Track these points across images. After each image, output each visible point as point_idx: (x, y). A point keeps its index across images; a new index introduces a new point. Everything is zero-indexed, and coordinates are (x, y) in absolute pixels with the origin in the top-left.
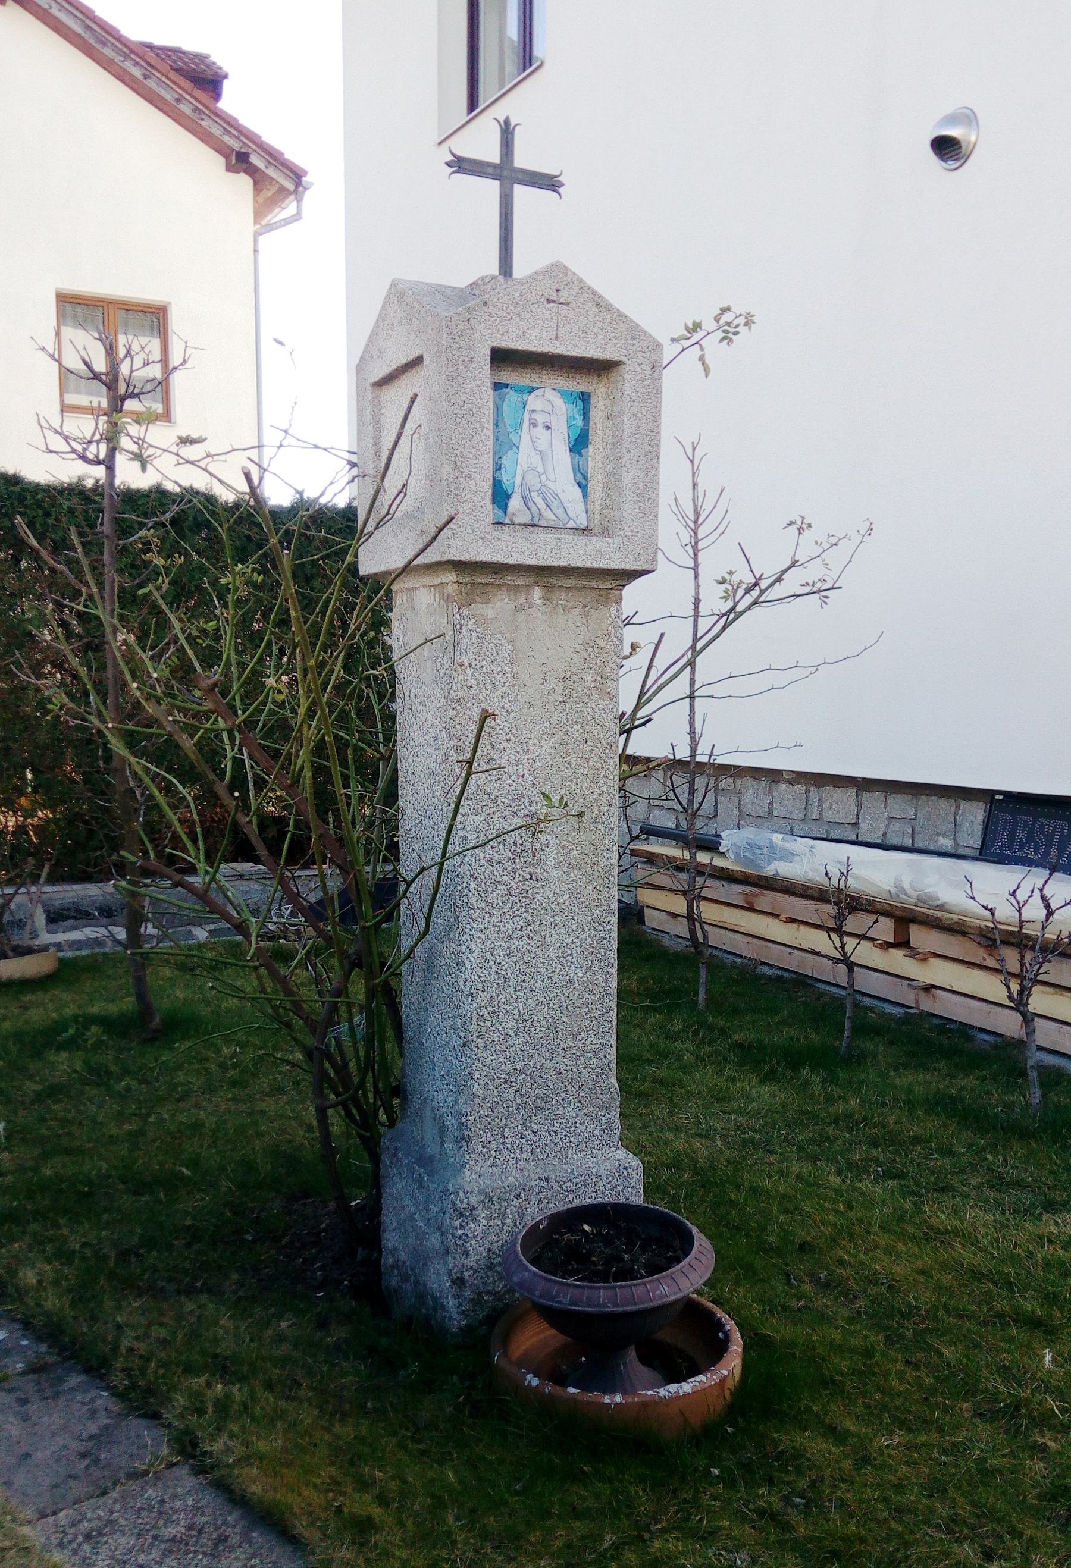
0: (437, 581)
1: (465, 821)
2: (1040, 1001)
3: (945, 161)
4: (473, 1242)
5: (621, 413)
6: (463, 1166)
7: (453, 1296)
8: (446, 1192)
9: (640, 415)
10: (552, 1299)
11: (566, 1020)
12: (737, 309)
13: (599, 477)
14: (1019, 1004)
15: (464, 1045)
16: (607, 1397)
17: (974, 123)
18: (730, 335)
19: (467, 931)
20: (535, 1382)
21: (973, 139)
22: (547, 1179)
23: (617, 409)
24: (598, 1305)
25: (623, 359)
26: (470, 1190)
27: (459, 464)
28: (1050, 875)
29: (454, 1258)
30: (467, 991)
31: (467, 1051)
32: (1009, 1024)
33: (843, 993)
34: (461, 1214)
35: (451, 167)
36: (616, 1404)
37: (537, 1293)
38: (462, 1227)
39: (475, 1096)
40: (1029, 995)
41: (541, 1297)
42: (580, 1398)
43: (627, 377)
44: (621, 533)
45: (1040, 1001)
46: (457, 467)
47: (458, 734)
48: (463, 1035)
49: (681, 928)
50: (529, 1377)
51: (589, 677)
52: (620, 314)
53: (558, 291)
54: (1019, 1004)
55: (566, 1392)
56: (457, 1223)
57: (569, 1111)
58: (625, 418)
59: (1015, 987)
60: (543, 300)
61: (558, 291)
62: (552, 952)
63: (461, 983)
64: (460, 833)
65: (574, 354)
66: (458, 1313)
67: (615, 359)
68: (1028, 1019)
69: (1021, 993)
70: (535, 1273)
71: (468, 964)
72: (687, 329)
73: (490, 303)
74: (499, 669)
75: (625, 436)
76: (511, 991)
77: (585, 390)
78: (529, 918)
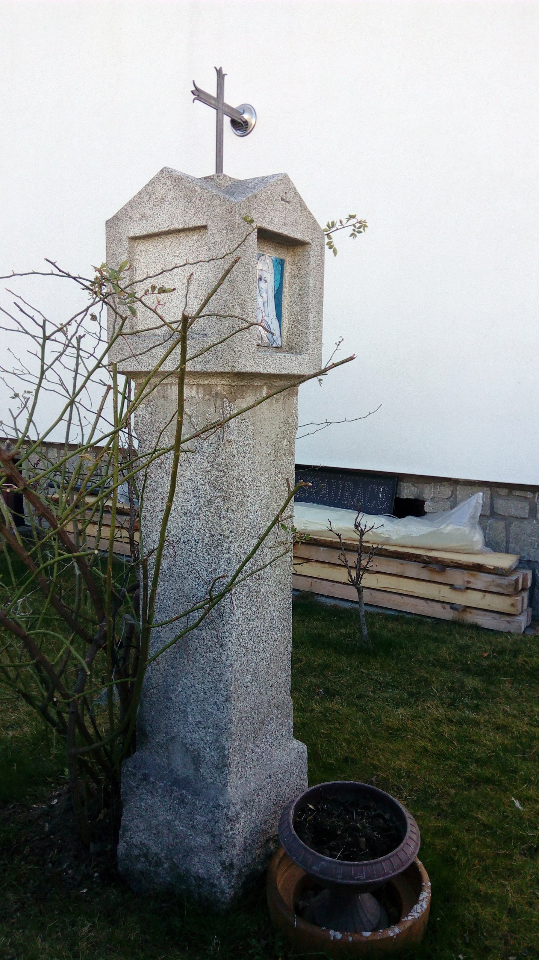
0: (207, 382)
1: (229, 547)
2: (367, 580)
3: (236, 130)
4: (238, 837)
5: (307, 275)
6: (225, 785)
7: (225, 877)
8: (218, 806)
9: (316, 278)
10: (352, 878)
11: (272, 666)
12: (359, 218)
13: (287, 314)
14: (356, 583)
15: (226, 701)
16: (390, 932)
17: (254, 115)
18: (356, 233)
19: (230, 622)
20: (339, 936)
21: (253, 123)
22: (270, 776)
23: (303, 272)
24: (385, 874)
25: (311, 241)
26: (235, 801)
27: (243, 305)
28: (359, 514)
29: (227, 852)
30: (228, 663)
31: (228, 704)
32: (352, 593)
33: (357, 606)
34: (231, 820)
35: (194, 94)
36: (397, 935)
37: (340, 876)
38: (232, 829)
39: (232, 734)
40: (361, 578)
41: (344, 878)
42: (375, 938)
43: (312, 253)
44: (308, 352)
45: (367, 580)
46: (242, 308)
47: (225, 488)
48: (225, 694)
49: (126, 549)
50: (332, 932)
51: (285, 443)
52: (310, 213)
53: (286, 193)
54: (356, 583)
55: (362, 936)
56: (228, 828)
57: (273, 725)
58: (311, 279)
59: (354, 574)
60: (280, 198)
61: (286, 193)
62: (267, 624)
63: (224, 658)
64: (226, 556)
65: (292, 236)
66: (229, 888)
67: (308, 241)
68: (359, 591)
69: (358, 578)
70: (331, 862)
71: (230, 645)
72: (328, 226)
73: (258, 196)
74: (247, 442)
75: (310, 291)
76: (249, 656)
77: (282, 258)
78: (258, 605)
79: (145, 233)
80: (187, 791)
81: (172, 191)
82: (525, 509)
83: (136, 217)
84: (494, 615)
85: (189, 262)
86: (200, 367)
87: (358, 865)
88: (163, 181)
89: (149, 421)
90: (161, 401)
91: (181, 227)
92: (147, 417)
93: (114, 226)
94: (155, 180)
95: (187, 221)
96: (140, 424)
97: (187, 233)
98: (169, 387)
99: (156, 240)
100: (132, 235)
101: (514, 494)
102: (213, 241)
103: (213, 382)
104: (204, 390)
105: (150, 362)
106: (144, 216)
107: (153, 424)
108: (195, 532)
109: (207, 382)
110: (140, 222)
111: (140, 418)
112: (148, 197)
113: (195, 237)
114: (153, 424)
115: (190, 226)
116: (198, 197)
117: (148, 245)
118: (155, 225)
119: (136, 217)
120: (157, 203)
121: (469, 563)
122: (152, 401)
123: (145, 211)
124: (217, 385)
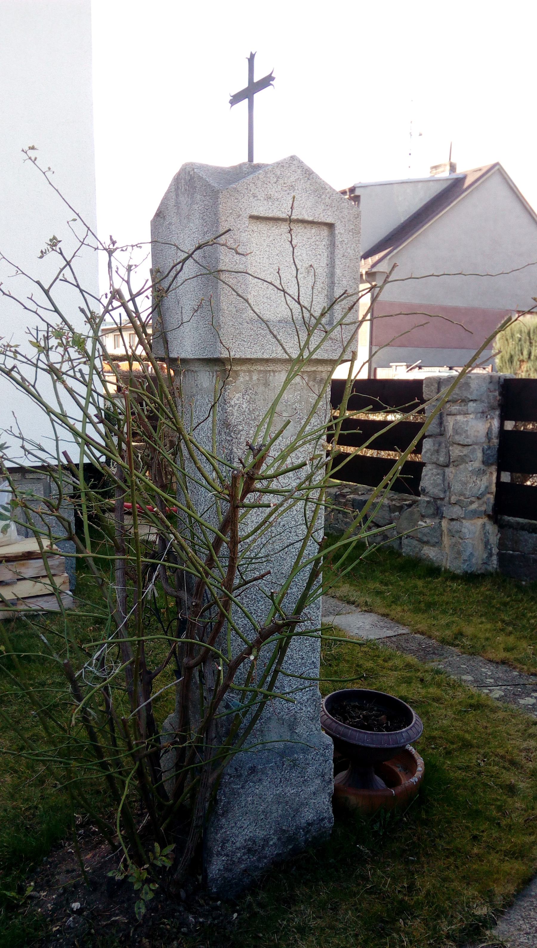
0: (314, 369)
79: (271, 215)
80: (297, 753)
81: (302, 181)
82: (40, 491)
83: (261, 196)
84: (45, 598)
85: (228, 244)
86: (326, 355)
87: (394, 734)
88: (293, 168)
89: (247, 410)
90: (261, 389)
91: (310, 219)
92: (244, 406)
93: (232, 198)
94: (284, 164)
95: (317, 216)
96: (235, 414)
97: (306, 225)
98: (272, 374)
99: (271, 223)
100: (255, 214)
101: (27, 477)
102: (341, 240)
103: (320, 368)
104: (309, 376)
105: (274, 349)
106: (269, 198)
107: (251, 413)
108: (295, 512)
109: (314, 369)
110: (265, 202)
111: (236, 408)
112: (276, 179)
113: (313, 231)
114: (251, 413)
115: (320, 221)
116: (328, 196)
117: (263, 227)
118: (283, 210)
119: (261, 196)
120: (285, 189)
121: (18, 553)
122: (251, 389)
123: (272, 193)
124: (322, 372)
